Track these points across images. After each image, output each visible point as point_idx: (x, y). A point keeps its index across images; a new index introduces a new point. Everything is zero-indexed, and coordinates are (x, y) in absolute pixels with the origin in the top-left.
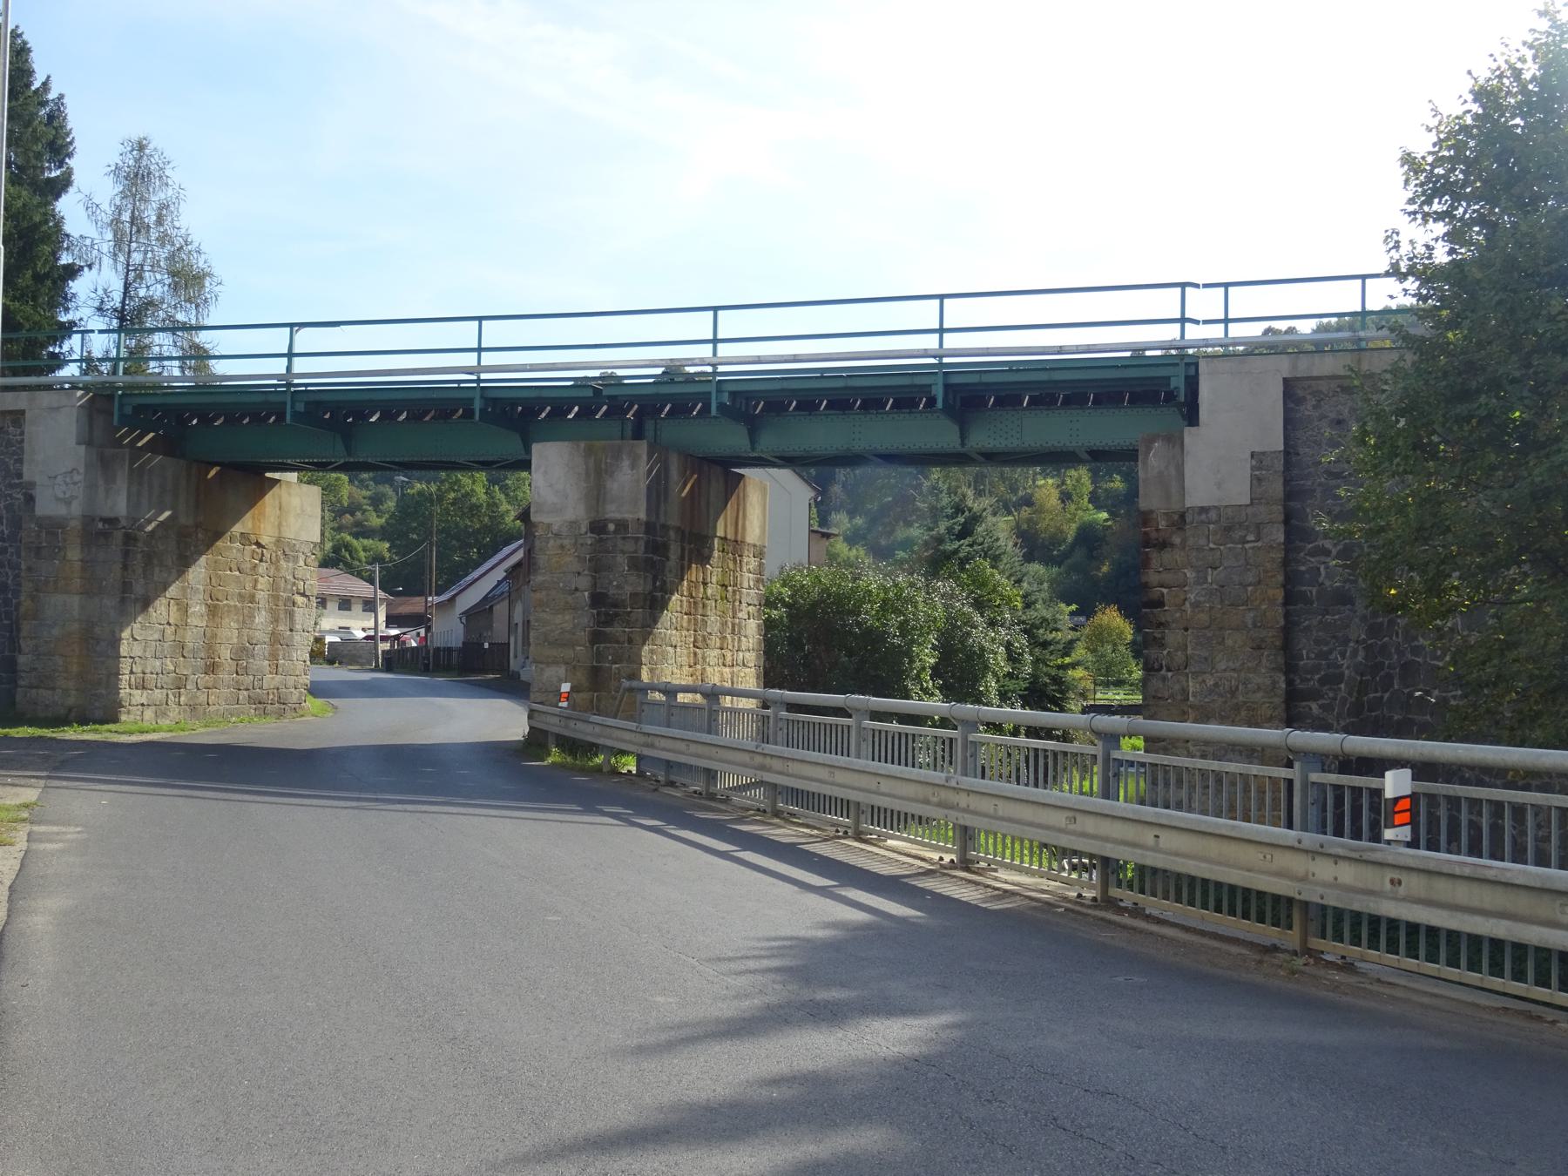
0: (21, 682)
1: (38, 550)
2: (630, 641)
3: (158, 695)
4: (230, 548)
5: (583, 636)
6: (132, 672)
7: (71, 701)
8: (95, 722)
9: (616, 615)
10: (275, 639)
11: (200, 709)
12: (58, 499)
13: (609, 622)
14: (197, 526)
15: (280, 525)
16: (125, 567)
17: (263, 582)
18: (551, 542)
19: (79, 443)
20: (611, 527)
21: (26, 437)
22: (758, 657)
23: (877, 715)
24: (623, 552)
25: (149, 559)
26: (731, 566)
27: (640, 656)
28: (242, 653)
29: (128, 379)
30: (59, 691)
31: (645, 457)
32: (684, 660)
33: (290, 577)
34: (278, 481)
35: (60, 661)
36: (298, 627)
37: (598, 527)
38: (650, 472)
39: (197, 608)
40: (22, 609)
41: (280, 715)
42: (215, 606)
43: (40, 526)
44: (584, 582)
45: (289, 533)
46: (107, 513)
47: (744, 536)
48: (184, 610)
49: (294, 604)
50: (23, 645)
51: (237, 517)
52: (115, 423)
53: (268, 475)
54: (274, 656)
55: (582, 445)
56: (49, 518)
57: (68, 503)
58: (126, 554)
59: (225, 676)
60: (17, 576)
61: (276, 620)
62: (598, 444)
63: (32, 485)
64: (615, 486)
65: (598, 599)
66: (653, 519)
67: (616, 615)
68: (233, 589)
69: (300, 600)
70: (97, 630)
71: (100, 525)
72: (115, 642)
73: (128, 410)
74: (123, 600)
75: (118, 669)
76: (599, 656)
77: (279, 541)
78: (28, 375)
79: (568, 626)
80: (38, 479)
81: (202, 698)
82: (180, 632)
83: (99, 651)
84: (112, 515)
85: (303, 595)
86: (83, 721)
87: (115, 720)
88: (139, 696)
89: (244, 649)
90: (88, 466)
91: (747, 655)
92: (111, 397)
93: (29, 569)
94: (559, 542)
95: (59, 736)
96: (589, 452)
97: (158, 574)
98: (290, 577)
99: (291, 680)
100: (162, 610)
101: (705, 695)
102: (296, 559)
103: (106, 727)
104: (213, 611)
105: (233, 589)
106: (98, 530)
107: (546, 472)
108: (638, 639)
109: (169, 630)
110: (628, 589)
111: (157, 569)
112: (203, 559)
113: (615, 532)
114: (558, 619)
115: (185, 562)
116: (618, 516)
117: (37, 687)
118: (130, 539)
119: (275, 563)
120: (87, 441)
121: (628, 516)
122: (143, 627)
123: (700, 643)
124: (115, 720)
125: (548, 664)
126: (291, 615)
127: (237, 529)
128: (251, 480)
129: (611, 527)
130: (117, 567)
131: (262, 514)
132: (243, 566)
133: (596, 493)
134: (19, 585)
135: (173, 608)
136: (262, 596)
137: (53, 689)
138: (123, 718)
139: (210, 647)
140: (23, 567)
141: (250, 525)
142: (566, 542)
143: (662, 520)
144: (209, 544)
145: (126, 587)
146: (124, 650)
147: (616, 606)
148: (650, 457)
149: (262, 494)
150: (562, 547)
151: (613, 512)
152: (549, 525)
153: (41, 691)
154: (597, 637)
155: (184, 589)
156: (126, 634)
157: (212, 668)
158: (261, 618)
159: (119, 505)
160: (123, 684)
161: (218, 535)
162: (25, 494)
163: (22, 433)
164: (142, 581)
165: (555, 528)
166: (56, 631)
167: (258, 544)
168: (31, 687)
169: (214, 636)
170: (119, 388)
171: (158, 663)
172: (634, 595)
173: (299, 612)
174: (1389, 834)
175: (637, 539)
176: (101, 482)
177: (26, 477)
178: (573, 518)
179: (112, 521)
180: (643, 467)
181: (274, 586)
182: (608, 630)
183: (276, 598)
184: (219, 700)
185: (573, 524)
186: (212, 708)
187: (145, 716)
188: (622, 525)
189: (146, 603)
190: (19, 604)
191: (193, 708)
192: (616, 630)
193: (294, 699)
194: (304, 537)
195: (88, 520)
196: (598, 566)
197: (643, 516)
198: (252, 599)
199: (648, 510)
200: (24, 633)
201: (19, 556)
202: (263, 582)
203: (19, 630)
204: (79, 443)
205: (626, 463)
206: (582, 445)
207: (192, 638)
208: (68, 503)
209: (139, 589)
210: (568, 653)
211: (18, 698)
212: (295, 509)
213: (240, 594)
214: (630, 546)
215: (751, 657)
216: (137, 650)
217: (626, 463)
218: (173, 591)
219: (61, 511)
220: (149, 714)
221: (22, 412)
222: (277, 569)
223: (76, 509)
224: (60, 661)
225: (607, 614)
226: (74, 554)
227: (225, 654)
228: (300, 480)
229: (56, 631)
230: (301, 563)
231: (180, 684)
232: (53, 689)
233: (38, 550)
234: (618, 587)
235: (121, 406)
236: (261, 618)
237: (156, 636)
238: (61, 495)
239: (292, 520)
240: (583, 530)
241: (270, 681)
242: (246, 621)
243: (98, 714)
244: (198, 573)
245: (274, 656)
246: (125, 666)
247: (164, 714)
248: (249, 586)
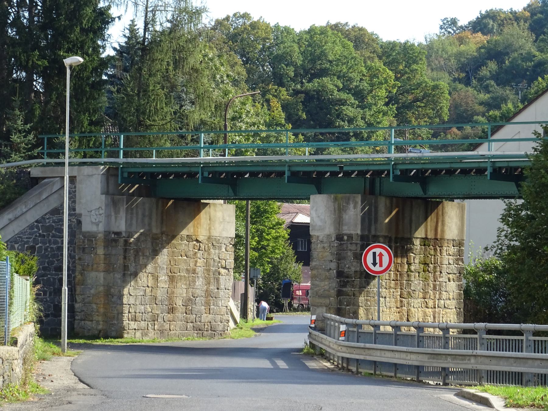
0: (77, 318)
1: (84, 249)
2: (354, 295)
3: (143, 324)
4: (180, 244)
5: (333, 292)
6: (129, 312)
7: (100, 327)
8: (111, 338)
9: (348, 282)
10: (208, 294)
11: (166, 332)
12: (92, 223)
13: (345, 286)
14: (162, 233)
15: (210, 228)
16: (125, 258)
17: (200, 262)
18: (319, 245)
19: (102, 194)
20: (345, 238)
21: (77, 189)
22: (459, 303)
23: (490, 332)
24: (351, 250)
25: (136, 255)
26: (432, 252)
27: (358, 302)
28: (189, 302)
29: (125, 160)
30: (94, 322)
31: (360, 203)
32: (393, 304)
33: (217, 259)
34: (207, 204)
35: (94, 306)
36: (222, 287)
37: (339, 238)
38: (363, 209)
39: (163, 278)
40: (77, 280)
41: (212, 337)
42: (173, 276)
43: (85, 237)
44: (333, 265)
45: (215, 233)
46: (116, 230)
47: (443, 231)
48: (156, 279)
49: (219, 274)
50: (77, 299)
51: (184, 225)
52: (119, 182)
53: (202, 201)
54: (207, 304)
55: (332, 196)
56: (89, 232)
57: (97, 225)
58: (125, 251)
59: (180, 314)
60: (74, 262)
61: (209, 283)
62: (340, 196)
63: (80, 215)
64: (347, 217)
65: (340, 274)
66: (366, 233)
67: (348, 282)
68: (183, 266)
69: (223, 271)
70: (112, 290)
71: (113, 236)
72: (121, 296)
73: (126, 175)
74: (124, 275)
75: (123, 310)
76: (340, 302)
77: (209, 238)
78: (70, 199)
79: (327, 287)
80: (83, 212)
81: (167, 326)
82: (154, 291)
83: (113, 299)
84: (118, 231)
85: (225, 268)
86: (106, 337)
87: (121, 337)
88: (133, 325)
89: (190, 300)
90: (107, 205)
91: (448, 302)
92: (117, 169)
93: (80, 259)
94: (322, 245)
95: (95, 343)
96: (336, 199)
97: (142, 261)
98: (217, 259)
99: (218, 318)
100: (144, 279)
101: (441, 329)
102: (220, 248)
103: (117, 340)
104: (172, 279)
105: (183, 266)
106: (112, 239)
107: (316, 210)
108: (357, 293)
109: (148, 290)
110: (353, 269)
111: (141, 258)
112: (165, 251)
113: (348, 240)
114: (322, 284)
115: (156, 252)
116: (348, 232)
117: (84, 320)
118: (126, 242)
119: (207, 251)
120: (106, 192)
121: (352, 232)
122: (135, 289)
123: (405, 296)
124: (121, 337)
125: (318, 306)
126: (218, 280)
127: (184, 233)
128: (193, 206)
129: (345, 238)
130: (121, 257)
131: (199, 223)
132: (188, 254)
133: (339, 221)
134: (75, 267)
135: (150, 278)
136: (200, 270)
137: (92, 321)
138: (125, 336)
139: (170, 297)
140: (77, 258)
141: (192, 230)
142: (326, 245)
143: (373, 233)
144: (168, 242)
145: (126, 268)
146: (125, 301)
147: (347, 277)
148: (362, 202)
149: (199, 211)
150: (324, 248)
151: (346, 230)
152: (318, 237)
153: (86, 322)
154: (340, 293)
155: (156, 268)
156: (126, 291)
157: (172, 310)
158: (200, 283)
159: (121, 225)
160: (125, 318)
161: (174, 237)
162: (77, 220)
163: (75, 187)
164: (134, 264)
165: (320, 238)
166: (92, 291)
167: (197, 241)
168: (81, 320)
169: (173, 293)
170: (121, 164)
171: (142, 307)
172: (356, 272)
173: (222, 279)
174: (340, 338)
175: (356, 244)
176: (113, 214)
177: (77, 211)
178: (329, 233)
179: (118, 234)
180: (359, 207)
181: (207, 264)
182: (344, 289)
183: (208, 270)
184: (176, 327)
185: (329, 236)
186: (172, 332)
187: (133, 332)
188: (350, 237)
189: (135, 275)
190: (75, 277)
191: (162, 332)
192: (348, 289)
193: (221, 328)
194: (225, 234)
195: (107, 233)
196: (340, 257)
197: (359, 232)
198: (194, 271)
199: (362, 229)
200: (78, 292)
201: (75, 252)
202: (200, 262)
203: (75, 291)
204: (102, 194)
205: (351, 206)
206: (332, 196)
207: (160, 294)
208: (97, 225)
209: (132, 269)
210: (327, 301)
211: (75, 326)
212: (220, 219)
213: (187, 269)
214: (353, 247)
215: (452, 304)
216: (132, 301)
217: (351, 206)
218: (150, 268)
219: (94, 229)
220: (138, 334)
221: (75, 177)
222: (209, 254)
223: (101, 228)
224: (94, 306)
225: (344, 281)
226: (101, 251)
227: (179, 302)
228: (225, 203)
229: (92, 291)
230: (224, 250)
231: (154, 319)
232: (92, 321)
233: (84, 249)
234: (348, 268)
235: (122, 173)
236: (200, 283)
237: (142, 293)
238: (94, 221)
239: (217, 225)
240: (333, 239)
241: (206, 318)
242: (191, 284)
243: (114, 334)
244: (163, 257)
245: (207, 304)
246: (126, 309)
247: (146, 335)
248: (192, 265)
